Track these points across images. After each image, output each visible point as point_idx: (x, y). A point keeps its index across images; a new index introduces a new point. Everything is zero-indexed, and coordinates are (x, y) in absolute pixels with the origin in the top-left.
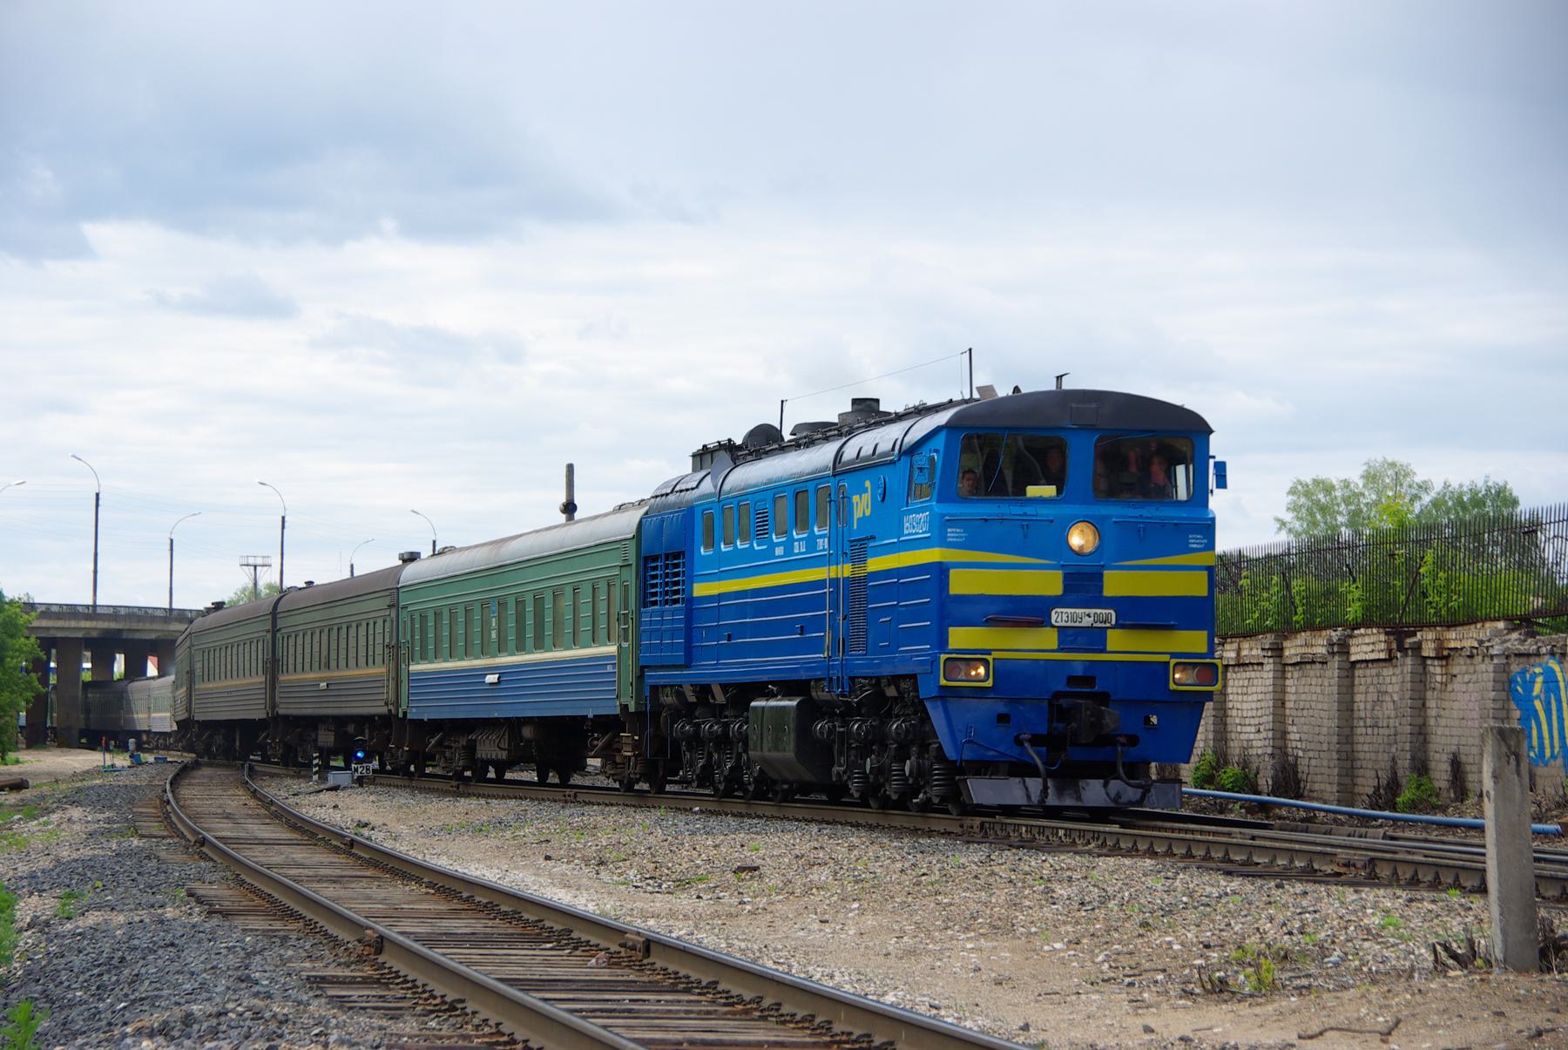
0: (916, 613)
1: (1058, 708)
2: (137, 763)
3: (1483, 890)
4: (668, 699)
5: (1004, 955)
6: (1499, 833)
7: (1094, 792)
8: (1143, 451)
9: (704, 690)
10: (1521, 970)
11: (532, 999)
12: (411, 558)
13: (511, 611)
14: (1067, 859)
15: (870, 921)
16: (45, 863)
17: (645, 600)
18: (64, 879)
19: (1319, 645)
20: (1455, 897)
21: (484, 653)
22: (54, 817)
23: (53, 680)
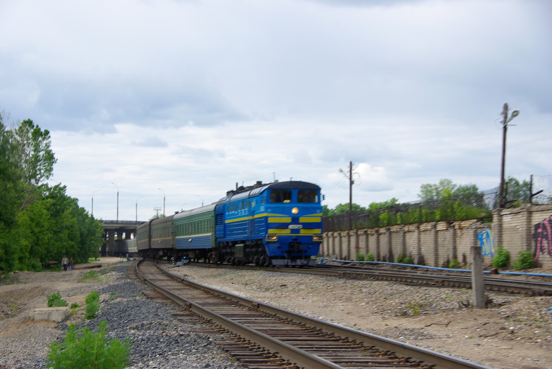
0: (262, 227)
1: (291, 245)
2: (129, 260)
3: (471, 288)
4: (221, 245)
5: (349, 306)
6: (476, 273)
7: (299, 262)
8: (308, 193)
9: (227, 243)
10: (481, 308)
11: (229, 319)
12: (177, 213)
13: (193, 226)
14: (365, 282)
15: (315, 298)
16: (106, 286)
17: (216, 224)
18: (111, 290)
19: (429, 226)
20: (464, 290)
21: (189, 234)
22: (109, 274)
23: (107, 239)
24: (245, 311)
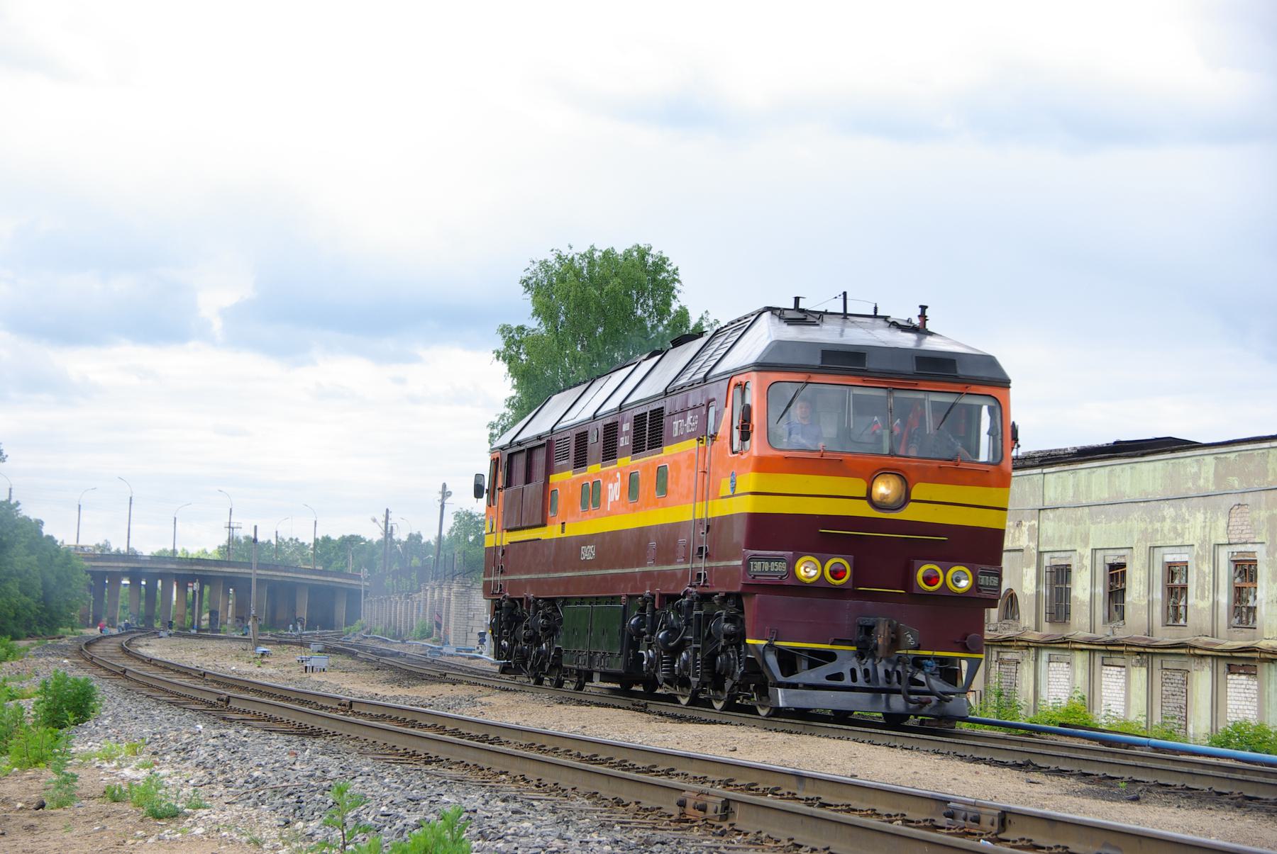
24: (204, 707)
